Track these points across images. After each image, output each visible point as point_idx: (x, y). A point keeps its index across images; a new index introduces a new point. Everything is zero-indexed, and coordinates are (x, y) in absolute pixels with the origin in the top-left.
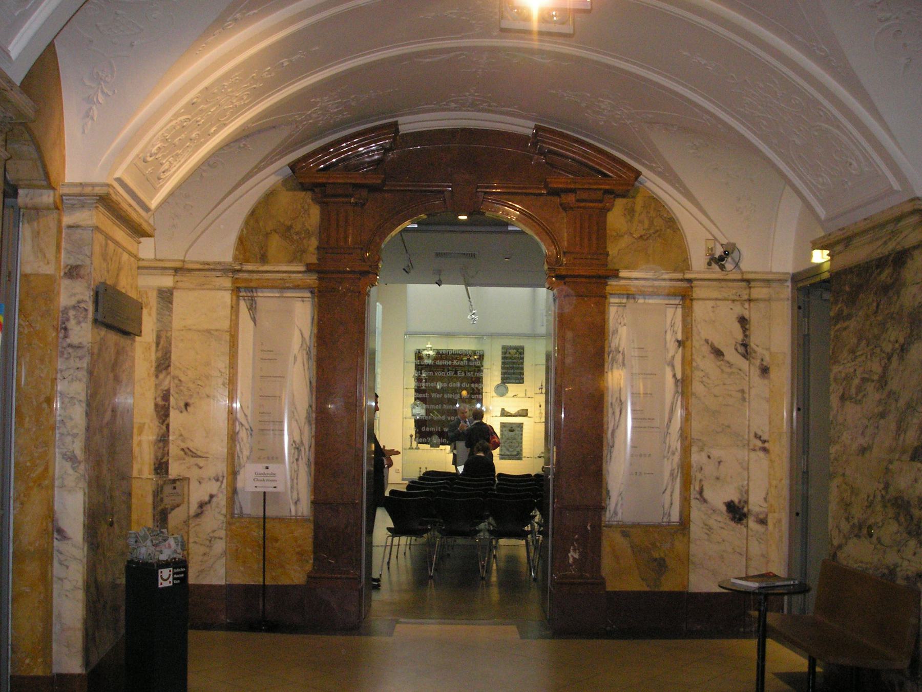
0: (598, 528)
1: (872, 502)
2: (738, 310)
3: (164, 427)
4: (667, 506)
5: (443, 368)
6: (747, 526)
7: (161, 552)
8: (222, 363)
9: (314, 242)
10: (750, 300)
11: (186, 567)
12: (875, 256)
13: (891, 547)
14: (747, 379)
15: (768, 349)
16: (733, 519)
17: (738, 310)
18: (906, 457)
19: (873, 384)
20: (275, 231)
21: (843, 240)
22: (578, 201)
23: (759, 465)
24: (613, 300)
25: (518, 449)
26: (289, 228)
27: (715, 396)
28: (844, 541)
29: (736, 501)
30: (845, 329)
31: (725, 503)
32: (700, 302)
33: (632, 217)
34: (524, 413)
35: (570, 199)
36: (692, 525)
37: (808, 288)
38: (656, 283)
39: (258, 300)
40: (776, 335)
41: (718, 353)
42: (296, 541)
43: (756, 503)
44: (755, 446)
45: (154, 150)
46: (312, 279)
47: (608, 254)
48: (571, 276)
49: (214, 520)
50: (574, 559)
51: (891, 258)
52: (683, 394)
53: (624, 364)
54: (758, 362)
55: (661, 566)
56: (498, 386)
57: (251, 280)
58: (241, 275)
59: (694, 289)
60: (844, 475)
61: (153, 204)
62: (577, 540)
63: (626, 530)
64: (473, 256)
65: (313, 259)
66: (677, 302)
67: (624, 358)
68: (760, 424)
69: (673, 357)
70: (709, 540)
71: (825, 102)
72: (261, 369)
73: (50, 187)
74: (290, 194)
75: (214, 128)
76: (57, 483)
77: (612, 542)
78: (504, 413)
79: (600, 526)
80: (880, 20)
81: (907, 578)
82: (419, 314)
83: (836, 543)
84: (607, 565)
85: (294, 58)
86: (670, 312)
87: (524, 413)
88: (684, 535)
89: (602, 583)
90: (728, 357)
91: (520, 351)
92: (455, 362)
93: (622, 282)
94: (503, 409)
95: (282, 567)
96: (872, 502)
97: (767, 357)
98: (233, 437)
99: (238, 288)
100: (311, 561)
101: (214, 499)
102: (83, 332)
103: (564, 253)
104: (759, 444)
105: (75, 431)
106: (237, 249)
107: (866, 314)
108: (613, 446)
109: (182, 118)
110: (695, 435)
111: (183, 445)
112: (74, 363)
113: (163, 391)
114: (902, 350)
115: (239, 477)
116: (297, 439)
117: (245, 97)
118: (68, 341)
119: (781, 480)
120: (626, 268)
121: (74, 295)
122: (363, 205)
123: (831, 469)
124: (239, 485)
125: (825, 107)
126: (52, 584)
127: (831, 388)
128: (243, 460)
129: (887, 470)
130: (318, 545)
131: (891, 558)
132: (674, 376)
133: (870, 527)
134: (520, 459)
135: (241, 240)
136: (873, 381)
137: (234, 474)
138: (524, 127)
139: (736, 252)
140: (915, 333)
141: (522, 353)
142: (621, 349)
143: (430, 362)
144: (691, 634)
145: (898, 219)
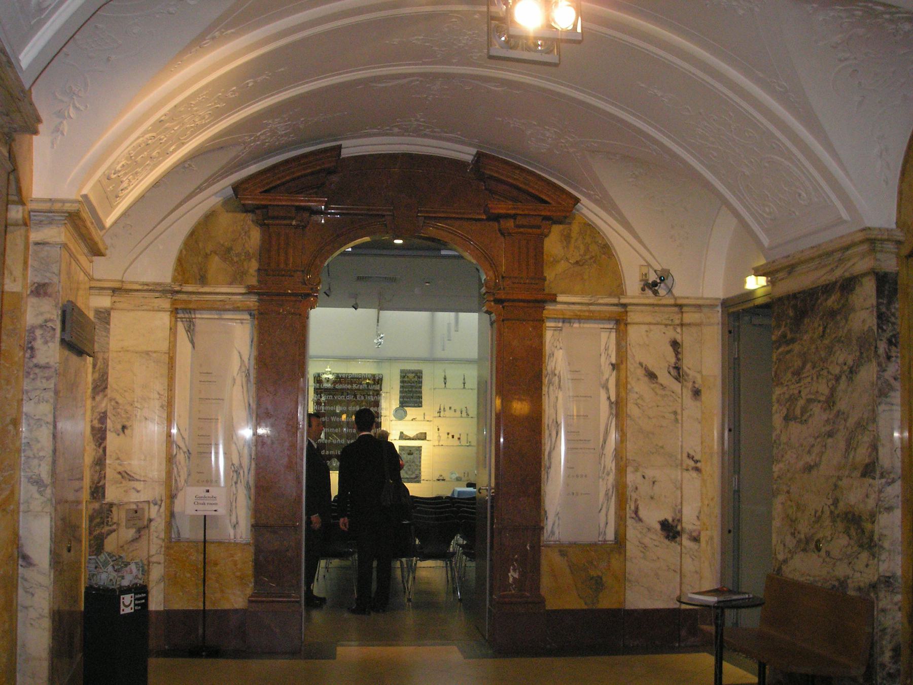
0: (537, 547)
1: (820, 517)
2: (671, 334)
3: (101, 451)
4: (602, 525)
5: (342, 392)
6: (681, 544)
7: (123, 577)
8: (159, 386)
9: (254, 265)
10: (682, 325)
11: (147, 592)
12: (822, 281)
13: (841, 560)
14: (680, 401)
15: (700, 372)
16: (667, 537)
17: (671, 334)
18: (857, 474)
19: (820, 405)
20: (215, 253)
21: (788, 266)
22: (518, 226)
23: (692, 484)
24: (548, 324)
25: (417, 472)
26: (229, 250)
27: (649, 418)
28: (790, 556)
29: (670, 520)
30: (789, 352)
31: (659, 522)
32: (636, 327)
33: (569, 243)
34: (422, 437)
35: (510, 224)
36: (628, 544)
37: (739, 313)
38: (592, 308)
39: (197, 322)
40: (707, 358)
41: (652, 376)
42: (236, 565)
43: (689, 520)
44: (688, 465)
45: (118, 167)
46: (252, 301)
47: (544, 279)
48: (509, 300)
49: (154, 545)
50: (514, 578)
51: (838, 284)
52: (617, 416)
53: (560, 387)
54: (690, 385)
55: (598, 584)
56: (396, 410)
57: (190, 302)
58: (180, 296)
59: (629, 314)
60: (788, 492)
61: (109, 222)
62: (516, 560)
63: (563, 549)
64: (393, 280)
65: (253, 281)
66: (611, 326)
67: (560, 381)
68: (693, 445)
69: (607, 380)
70: (645, 558)
71: (778, 134)
72: (200, 392)
73: (22, 202)
74: (230, 215)
75: (173, 147)
76: (22, 508)
77: (550, 561)
78: (402, 437)
79: (540, 546)
80: (840, 60)
81: (859, 589)
82: (340, 336)
83: (780, 557)
84: (546, 582)
85: (259, 79)
86: (604, 335)
87: (422, 437)
88: (620, 553)
89: (542, 601)
90: (661, 380)
91: (418, 375)
92: (354, 386)
93: (559, 307)
94: (402, 433)
95: (222, 591)
96: (820, 517)
97: (699, 381)
98: (170, 459)
99: (176, 309)
100: (252, 585)
101: (153, 524)
102: (50, 352)
103: (503, 277)
104: (692, 463)
105: (41, 454)
106: (176, 270)
107: (811, 338)
108: (549, 468)
109: (148, 136)
110: (630, 455)
111: (120, 469)
112: (41, 383)
113: (100, 413)
114: (851, 372)
115: (176, 501)
116: (236, 461)
117: (207, 117)
118: (35, 361)
119: (712, 499)
120: (563, 292)
121: (42, 314)
122: (304, 227)
123: (775, 486)
124: (177, 509)
125: (779, 140)
126: (17, 611)
127: (774, 408)
128: (181, 482)
129: (836, 486)
130: (259, 568)
131: (842, 570)
132: (609, 398)
133: (818, 541)
134: (419, 482)
135: (180, 261)
136: (819, 401)
137: (172, 497)
138: (466, 154)
139: (670, 278)
140: (865, 355)
141: (420, 377)
142: (557, 372)
143: (329, 385)
144: (628, 650)
145: (847, 248)
